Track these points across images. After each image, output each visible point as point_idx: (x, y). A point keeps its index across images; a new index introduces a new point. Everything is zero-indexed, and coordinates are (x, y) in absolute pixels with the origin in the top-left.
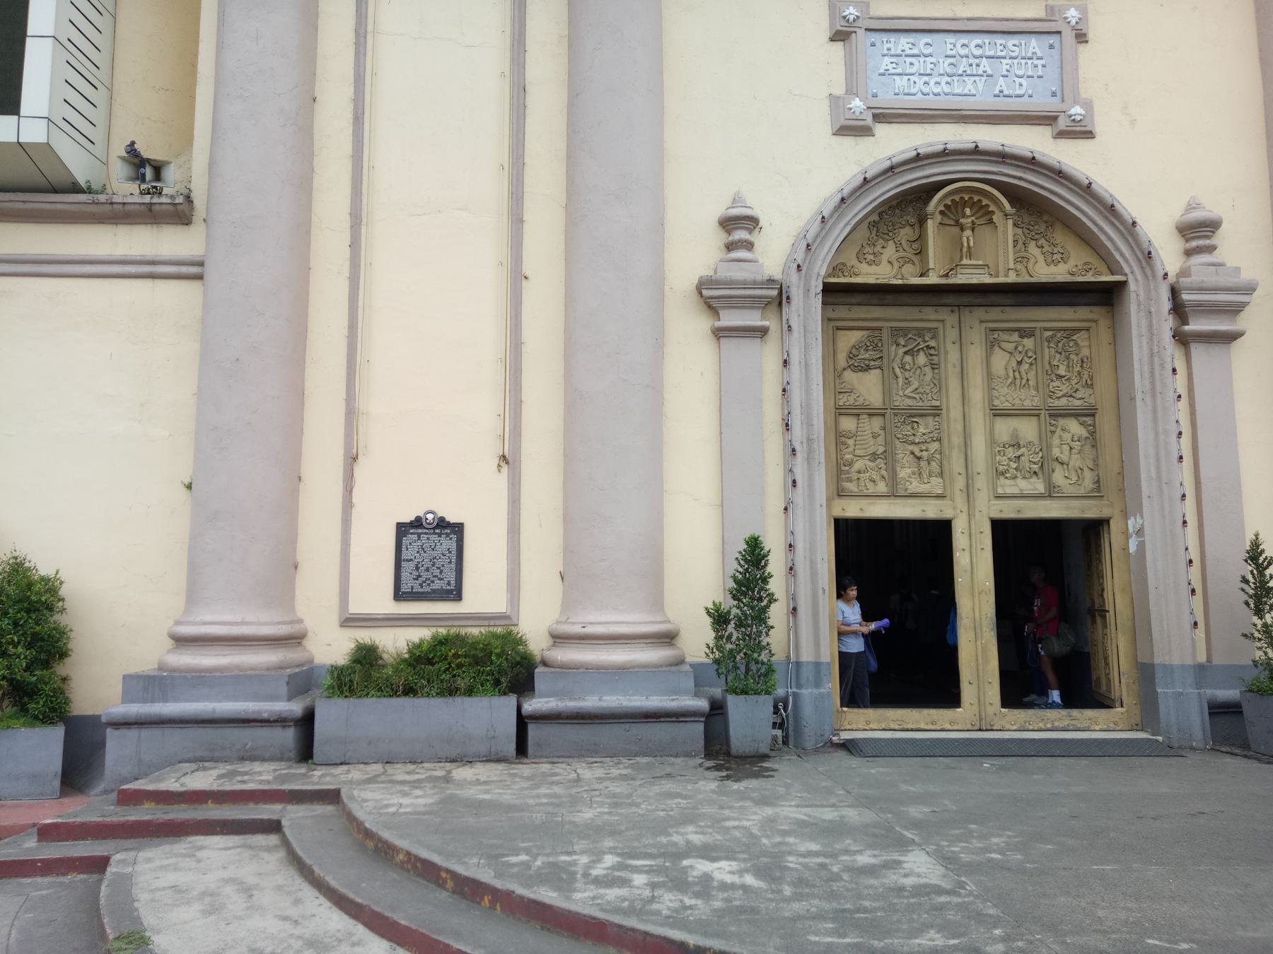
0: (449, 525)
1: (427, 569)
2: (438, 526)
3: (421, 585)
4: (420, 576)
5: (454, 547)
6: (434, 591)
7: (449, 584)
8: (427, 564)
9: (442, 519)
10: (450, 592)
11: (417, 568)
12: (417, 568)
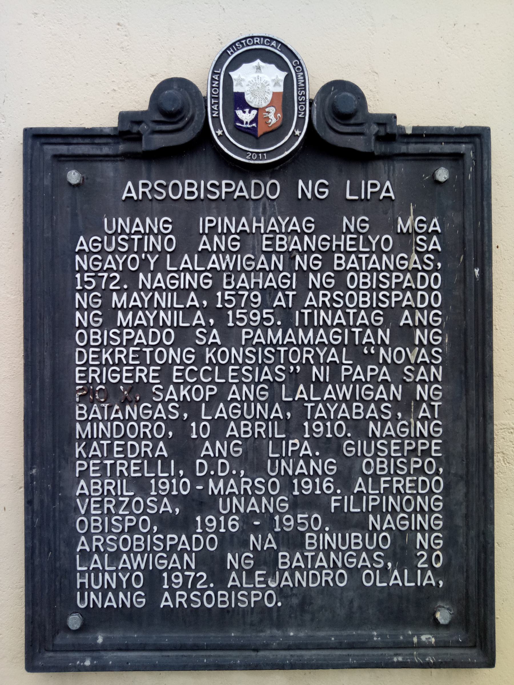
0: (391, 144)
1: (253, 458)
2: (314, 144)
3: (214, 568)
4: (199, 503)
5: (427, 304)
6: (300, 604)
7: (402, 552)
8: (248, 413)
9: (342, 102)
10: (406, 609)
11: (183, 451)
12: (183, 451)
